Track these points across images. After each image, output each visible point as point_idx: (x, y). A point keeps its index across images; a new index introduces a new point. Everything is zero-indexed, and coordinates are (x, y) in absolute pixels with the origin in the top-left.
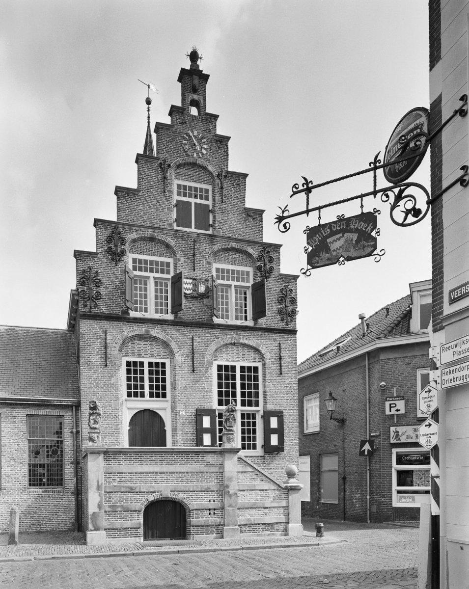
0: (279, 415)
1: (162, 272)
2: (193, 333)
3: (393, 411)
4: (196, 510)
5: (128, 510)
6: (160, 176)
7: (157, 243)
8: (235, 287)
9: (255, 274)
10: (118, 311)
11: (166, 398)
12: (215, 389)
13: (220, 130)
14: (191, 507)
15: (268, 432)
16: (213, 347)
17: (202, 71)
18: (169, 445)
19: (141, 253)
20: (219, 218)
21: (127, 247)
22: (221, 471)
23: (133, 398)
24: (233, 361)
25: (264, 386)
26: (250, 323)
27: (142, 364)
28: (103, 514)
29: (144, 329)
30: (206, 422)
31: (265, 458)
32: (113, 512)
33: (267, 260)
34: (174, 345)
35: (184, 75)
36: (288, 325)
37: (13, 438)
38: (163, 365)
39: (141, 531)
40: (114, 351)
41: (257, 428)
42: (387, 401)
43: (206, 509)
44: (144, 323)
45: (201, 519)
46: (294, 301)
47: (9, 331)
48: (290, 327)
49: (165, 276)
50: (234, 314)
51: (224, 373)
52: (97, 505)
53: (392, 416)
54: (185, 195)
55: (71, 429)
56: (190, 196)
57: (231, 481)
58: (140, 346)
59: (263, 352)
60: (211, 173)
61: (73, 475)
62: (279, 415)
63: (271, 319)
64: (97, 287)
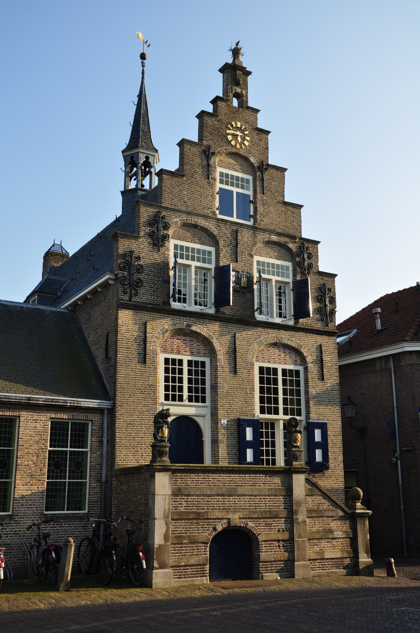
0: (323, 427)
1: (204, 262)
4: (264, 541)
5: (193, 541)
9: (294, 271)
10: (159, 301)
11: (205, 403)
12: (161, 384)
15: (311, 445)
18: (208, 461)
20: (260, 209)
21: (170, 232)
22: (289, 494)
24: (274, 362)
26: (211, 311)
27: (181, 362)
28: (171, 548)
29: (185, 323)
32: (178, 544)
35: (225, 69)
36: (328, 326)
37: (32, 448)
38: (203, 364)
41: (276, 439)
43: (275, 541)
44: (185, 316)
45: (270, 553)
46: (333, 300)
50: (193, 298)
51: (200, 369)
52: (163, 536)
54: (227, 183)
55: (100, 437)
56: (232, 185)
57: (300, 506)
59: (305, 354)
60: (252, 165)
62: (323, 427)
63: (312, 320)
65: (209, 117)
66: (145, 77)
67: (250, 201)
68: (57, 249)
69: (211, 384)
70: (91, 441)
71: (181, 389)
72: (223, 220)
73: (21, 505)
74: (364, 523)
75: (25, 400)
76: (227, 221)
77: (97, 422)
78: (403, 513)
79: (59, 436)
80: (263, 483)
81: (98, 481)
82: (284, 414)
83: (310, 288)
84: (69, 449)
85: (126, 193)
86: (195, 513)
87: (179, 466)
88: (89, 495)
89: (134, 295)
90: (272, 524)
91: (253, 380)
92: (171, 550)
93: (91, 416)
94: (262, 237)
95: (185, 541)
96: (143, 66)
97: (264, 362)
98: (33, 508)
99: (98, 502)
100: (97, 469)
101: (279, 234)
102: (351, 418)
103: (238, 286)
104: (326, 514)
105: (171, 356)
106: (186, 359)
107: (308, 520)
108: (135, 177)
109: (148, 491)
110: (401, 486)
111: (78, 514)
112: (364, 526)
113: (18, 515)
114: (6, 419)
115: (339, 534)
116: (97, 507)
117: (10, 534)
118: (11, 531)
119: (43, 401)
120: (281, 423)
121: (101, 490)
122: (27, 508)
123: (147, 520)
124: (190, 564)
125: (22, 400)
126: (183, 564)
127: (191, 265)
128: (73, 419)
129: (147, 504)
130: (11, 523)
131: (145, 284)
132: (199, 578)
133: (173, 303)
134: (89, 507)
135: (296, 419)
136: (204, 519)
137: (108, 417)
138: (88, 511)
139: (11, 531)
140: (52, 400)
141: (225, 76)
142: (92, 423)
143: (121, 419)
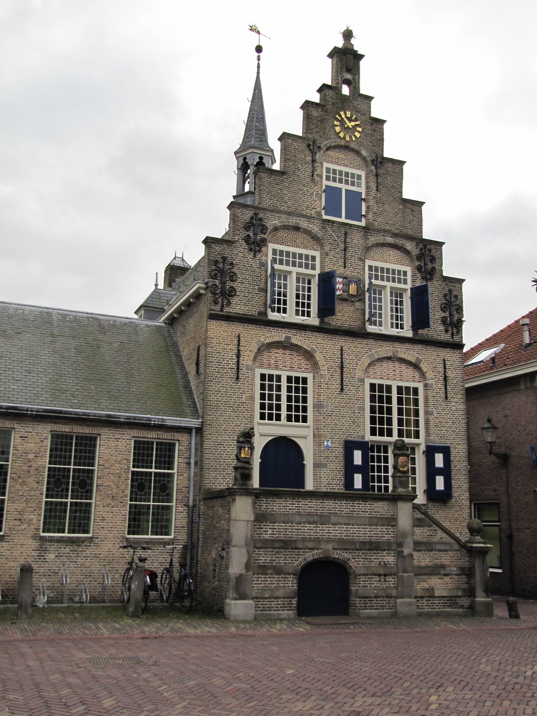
0: (446, 451)
1: (307, 267)
4: (363, 575)
5: (279, 571)
6: (308, 158)
7: (302, 232)
8: (390, 289)
10: (253, 310)
11: (307, 423)
13: (375, 113)
14: (358, 572)
15: (432, 472)
16: (366, 361)
17: (357, 51)
18: (309, 486)
19: (282, 244)
23: (266, 421)
25: (426, 413)
26: (409, 334)
29: (284, 335)
30: (358, 457)
31: (428, 507)
34: (318, 356)
35: (335, 53)
37: (113, 468)
39: (294, 601)
40: (247, 360)
43: (375, 575)
44: (284, 328)
46: (460, 309)
47: (91, 320)
48: (456, 339)
49: (310, 272)
52: (244, 565)
54: (334, 180)
56: (341, 181)
59: (425, 369)
60: (364, 159)
61: (186, 521)
62: (446, 451)
63: (436, 330)
64: (231, 281)
65: (313, 107)
66: (260, 72)
67: (362, 199)
68: (178, 263)
69: (314, 402)
72: (329, 221)
73: (102, 528)
75: (124, 419)
76: (333, 222)
77: (185, 443)
79: (143, 456)
80: (362, 512)
81: (185, 505)
82: (371, 435)
84: (153, 470)
86: (282, 541)
88: (175, 519)
89: (227, 305)
93: (178, 436)
94: (373, 239)
96: (259, 59)
97: (376, 378)
98: (114, 531)
99: (185, 527)
100: (184, 492)
101: (395, 235)
102: (491, 443)
103: (346, 294)
104: (438, 547)
107: (415, 554)
111: (163, 539)
113: (98, 538)
114: (86, 437)
116: (184, 532)
117: (90, 557)
118: (91, 554)
119: (124, 419)
122: (108, 531)
124: (274, 595)
125: (103, 417)
126: (267, 595)
127: (386, 286)
128: (158, 438)
130: (91, 546)
131: (238, 293)
132: (286, 612)
133: (370, 326)
134: (175, 532)
135: (403, 441)
136: (292, 549)
137: (196, 437)
139: (91, 554)
140: (135, 418)
141: (334, 62)
142: (179, 443)
143: (211, 439)
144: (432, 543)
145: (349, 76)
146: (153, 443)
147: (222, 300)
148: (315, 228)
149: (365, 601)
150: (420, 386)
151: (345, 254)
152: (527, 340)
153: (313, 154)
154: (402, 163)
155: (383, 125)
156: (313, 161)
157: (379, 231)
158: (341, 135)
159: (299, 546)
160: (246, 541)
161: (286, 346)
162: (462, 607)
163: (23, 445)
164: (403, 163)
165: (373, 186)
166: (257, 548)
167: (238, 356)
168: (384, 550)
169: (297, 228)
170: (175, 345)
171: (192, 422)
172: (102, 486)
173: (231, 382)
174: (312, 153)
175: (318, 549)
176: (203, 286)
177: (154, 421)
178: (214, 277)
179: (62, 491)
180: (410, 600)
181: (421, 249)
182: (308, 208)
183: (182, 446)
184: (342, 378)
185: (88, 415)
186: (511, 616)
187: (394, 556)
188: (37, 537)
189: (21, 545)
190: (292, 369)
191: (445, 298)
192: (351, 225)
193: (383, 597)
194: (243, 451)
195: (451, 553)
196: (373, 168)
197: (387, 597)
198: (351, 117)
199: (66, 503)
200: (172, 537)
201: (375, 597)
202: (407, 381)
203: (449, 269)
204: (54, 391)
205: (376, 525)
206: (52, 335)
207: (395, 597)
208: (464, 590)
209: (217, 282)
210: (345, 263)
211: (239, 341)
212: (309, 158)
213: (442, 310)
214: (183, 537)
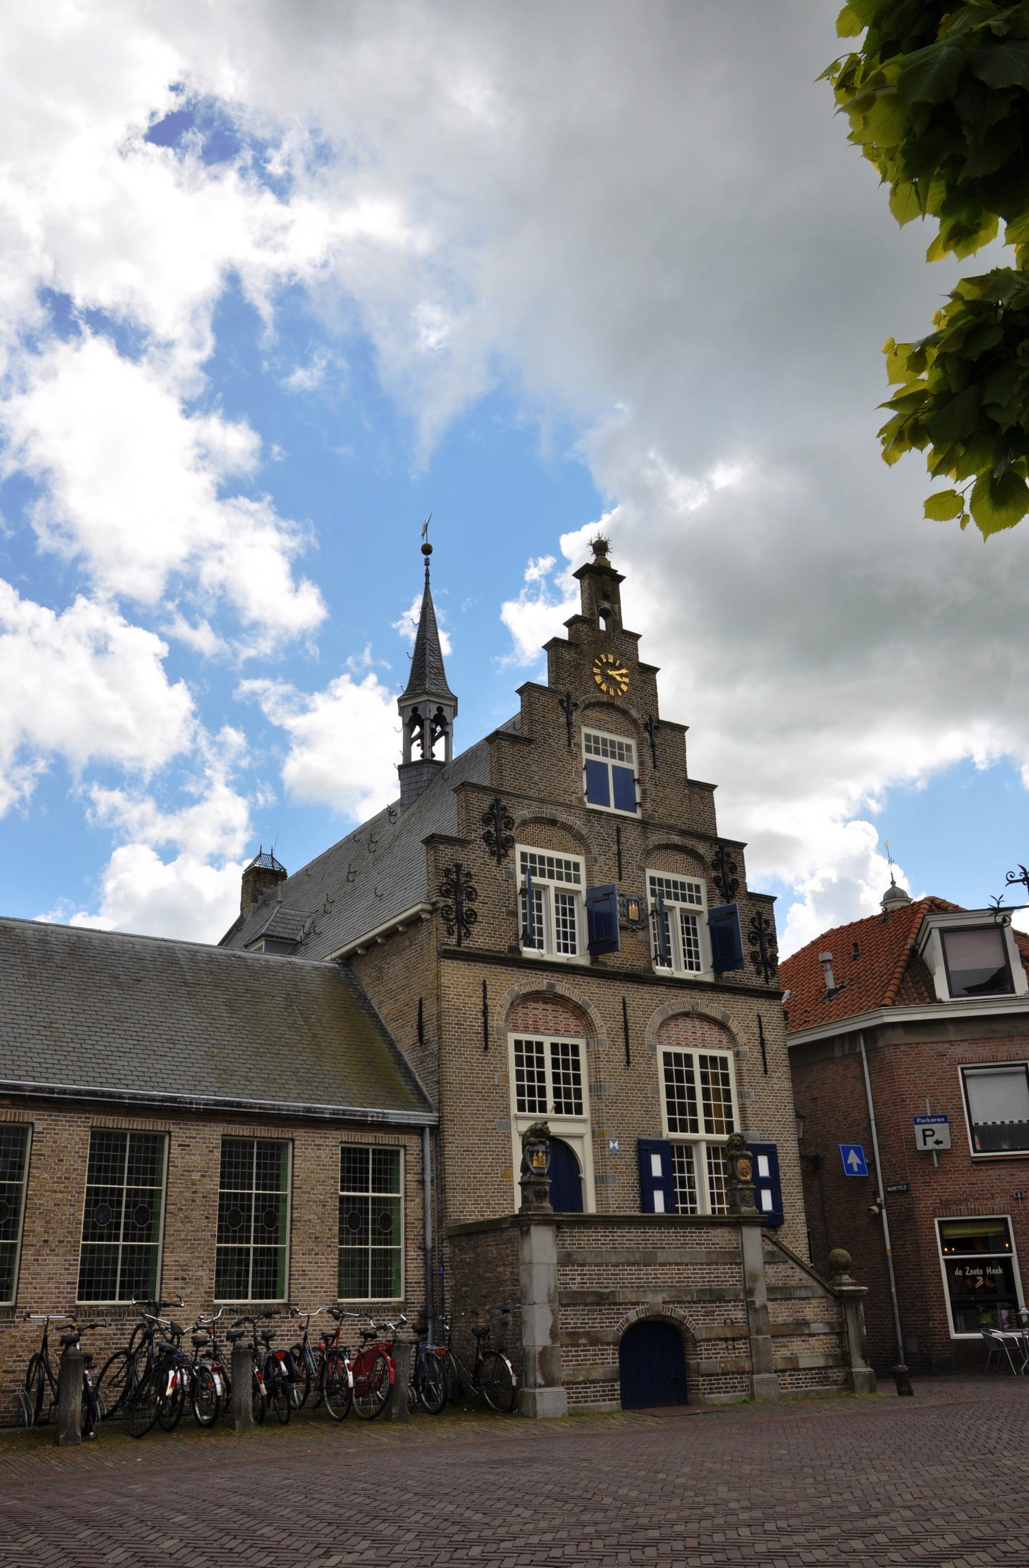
1: (569, 880)
2: (623, 992)
3: (931, 1145)
4: (705, 1340)
5: (594, 1340)
10: (501, 945)
14: (698, 1336)
16: (656, 1019)
18: (591, 1207)
19: (533, 844)
20: (652, 792)
24: (687, 1045)
25: (741, 1095)
27: (540, 1046)
29: (545, 981)
33: (727, 870)
34: (593, 1012)
37: (315, 1192)
38: (575, 1049)
39: (617, 1386)
40: (497, 1021)
42: (916, 1123)
43: (720, 1339)
44: (545, 970)
53: (929, 1153)
54: (597, 752)
56: (605, 754)
58: (536, 1012)
59: (734, 1030)
60: (634, 722)
64: (470, 900)
67: (635, 780)
68: (264, 864)
70: (406, 1181)
71: (542, 1092)
74: (857, 1309)
76: (601, 813)
78: (895, 1300)
81: (419, 1248)
82: (707, 1132)
83: (741, 924)
84: (370, 1194)
85: (406, 769)
86: (596, 1294)
87: (567, 1216)
90: (714, 1311)
91: (656, 1074)
92: (562, 1356)
93: (404, 1139)
94: (656, 838)
95: (583, 1341)
96: (427, 564)
101: (683, 833)
103: (624, 919)
104: (798, 1293)
105: (524, 1037)
106: (547, 1041)
107: (770, 1305)
108: (419, 741)
109: (518, 1259)
110: (889, 1254)
111: (390, 1303)
112: (857, 1313)
115: (818, 1327)
120: (703, 1147)
121: (425, 1263)
123: (519, 1308)
124: (591, 1378)
126: (581, 1379)
128: (375, 1144)
129: (517, 1280)
131: (480, 919)
132: (607, 1403)
136: (609, 1305)
138: (406, 1299)
141: (586, 584)
142: (406, 1150)
144: (790, 1288)
145: (607, 605)
146: (367, 1150)
147: (459, 929)
148: (577, 823)
149: (710, 1380)
150: (729, 1055)
151: (619, 860)
152: (831, 984)
153: (568, 713)
154: (685, 728)
155: (655, 674)
156: (569, 724)
157: (661, 826)
158: (604, 687)
159: (618, 1301)
160: (549, 1295)
161: (549, 998)
162: (835, 1383)
163: (183, 1158)
164: (686, 728)
165: (649, 763)
166: (563, 1305)
167: (485, 1013)
168: (729, 1301)
169: (552, 822)
170: (363, 998)
171: (426, 1118)
172: (299, 1221)
173: (477, 1054)
174: (566, 712)
175: (643, 1303)
176: (429, 907)
177: (372, 1117)
178: (445, 894)
179: (241, 1230)
180: (770, 1375)
181: (717, 853)
182: (566, 792)
183: (410, 1155)
184: (627, 1046)
185: (279, 1110)
186: (901, 1393)
187: (743, 1310)
188: (208, 1306)
189: (186, 1319)
190: (557, 1032)
191: (753, 925)
192: (624, 818)
193: (733, 1373)
194: (535, 1157)
195: (814, 1302)
196: (647, 735)
197: (739, 1373)
198: (615, 662)
199: (248, 1249)
200: (401, 1299)
201: (723, 1374)
202: (712, 1047)
203: (755, 881)
204: (218, 1072)
205: (717, 1264)
206: (186, 984)
207: (748, 1373)
208: (835, 1357)
209: (450, 902)
210: (620, 873)
211: (485, 991)
212: (563, 720)
213: (750, 941)
214: (418, 1298)
